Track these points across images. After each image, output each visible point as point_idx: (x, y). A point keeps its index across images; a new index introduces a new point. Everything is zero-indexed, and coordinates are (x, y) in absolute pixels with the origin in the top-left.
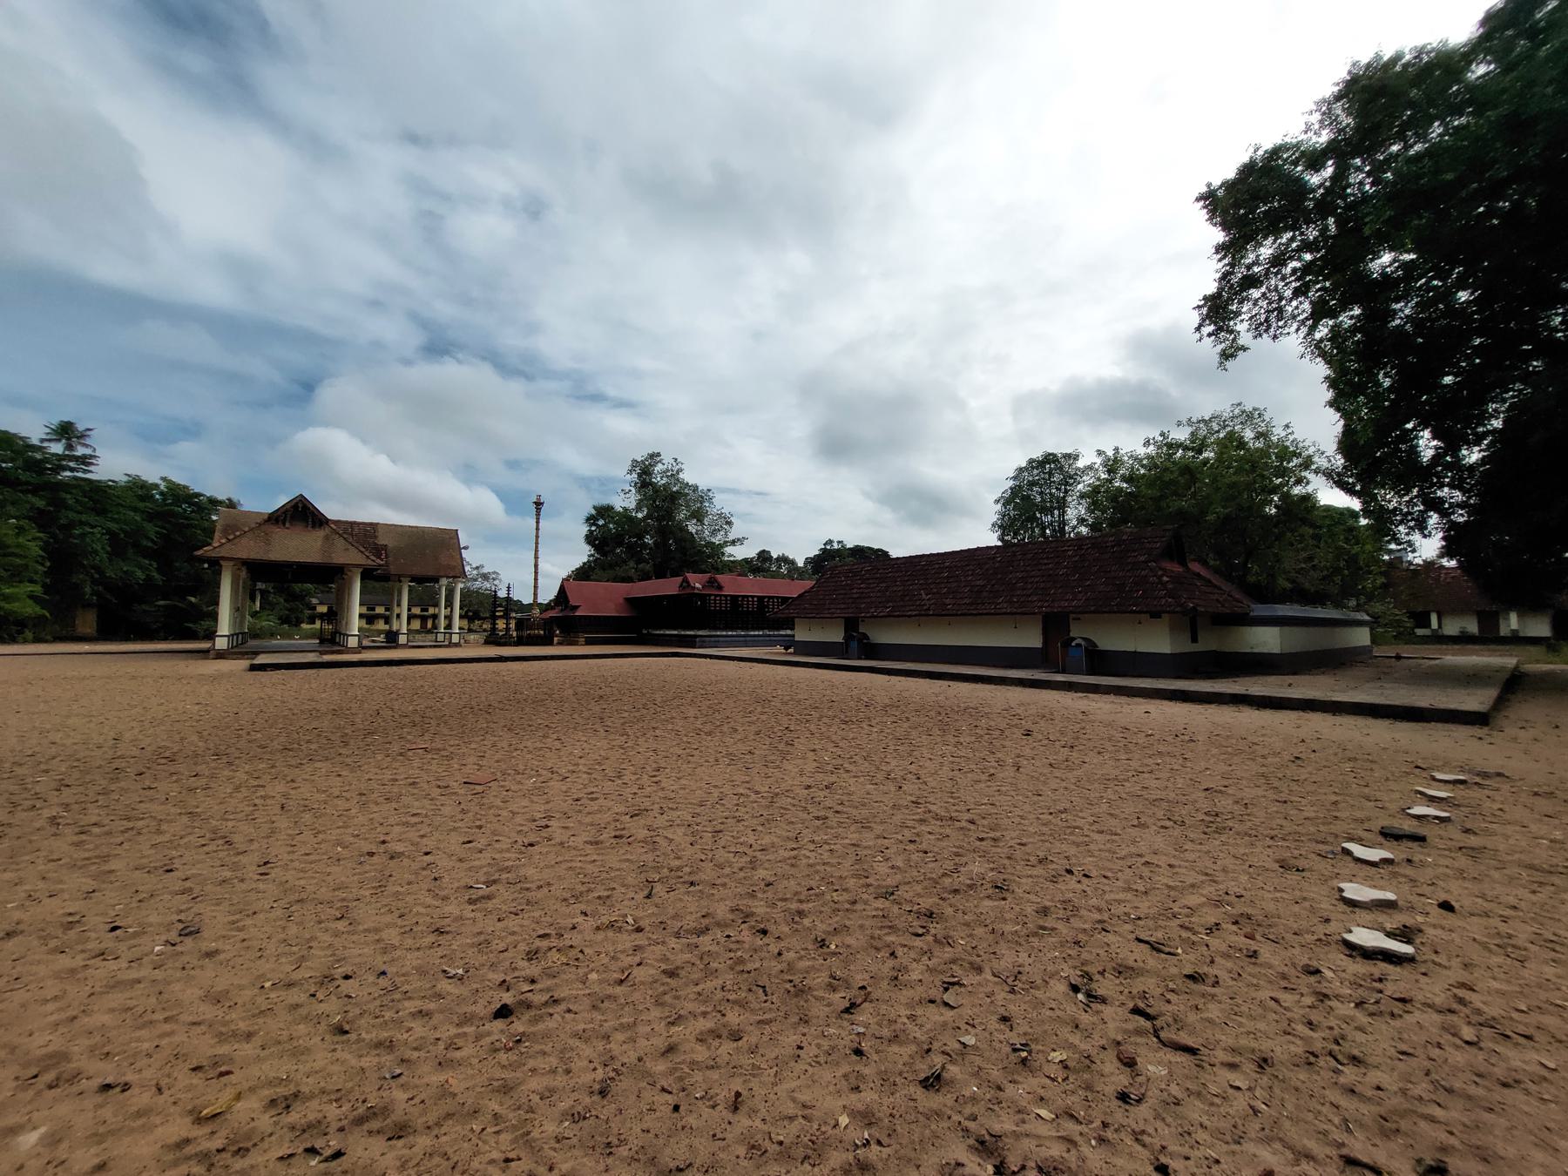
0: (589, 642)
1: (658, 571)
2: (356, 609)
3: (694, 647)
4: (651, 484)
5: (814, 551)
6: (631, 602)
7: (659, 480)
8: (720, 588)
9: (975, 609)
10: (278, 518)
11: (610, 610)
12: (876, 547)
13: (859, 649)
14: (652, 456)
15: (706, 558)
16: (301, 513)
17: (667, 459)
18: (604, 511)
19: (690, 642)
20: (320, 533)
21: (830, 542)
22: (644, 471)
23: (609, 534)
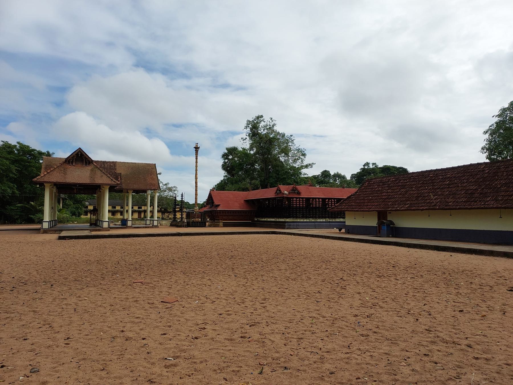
0: (225, 225)
1: (265, 185)
2: (107, 208)
3: (284, 228)
4: (258, 134)
5: (357, 170)
6: (248, 202)
7: (262, 131)
8: (299, 193)
9: (470, 204)
10: (69, 161)
11: (236, 206)
12: (398, 166)
13: (387, 231)
14: (258, 118)
15: (291, 176)
16: (80, 158)
17: (266, 118)
18: (232, 151)
19: (282, 225)
20: (89, 168)
21: (367, 164)
22: (254, 127)
23: (236, 164)
